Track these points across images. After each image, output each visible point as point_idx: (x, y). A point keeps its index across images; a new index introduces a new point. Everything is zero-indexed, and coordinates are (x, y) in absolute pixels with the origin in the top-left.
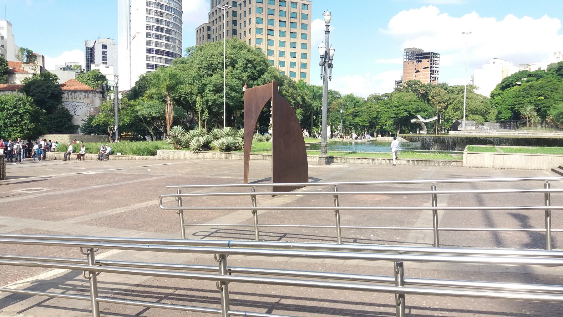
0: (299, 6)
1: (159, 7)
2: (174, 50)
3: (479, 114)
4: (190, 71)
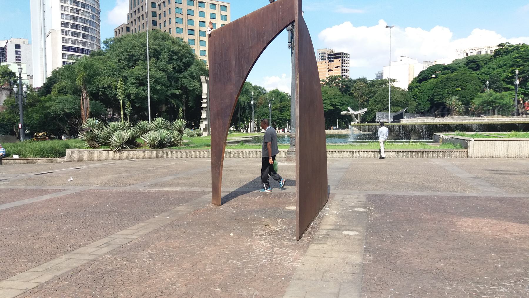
0: (218, 7)
1: (75, 4)
2: (92, 47)
3: (400, 106)
4: (108, 62)
